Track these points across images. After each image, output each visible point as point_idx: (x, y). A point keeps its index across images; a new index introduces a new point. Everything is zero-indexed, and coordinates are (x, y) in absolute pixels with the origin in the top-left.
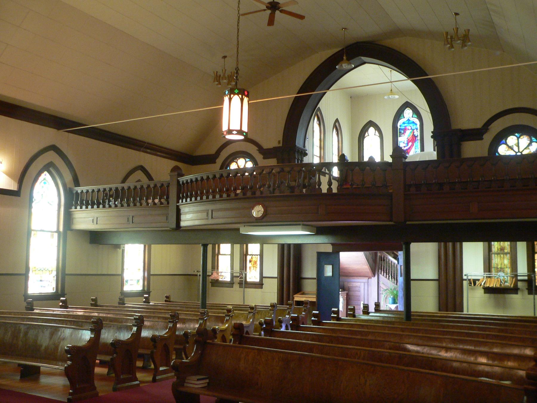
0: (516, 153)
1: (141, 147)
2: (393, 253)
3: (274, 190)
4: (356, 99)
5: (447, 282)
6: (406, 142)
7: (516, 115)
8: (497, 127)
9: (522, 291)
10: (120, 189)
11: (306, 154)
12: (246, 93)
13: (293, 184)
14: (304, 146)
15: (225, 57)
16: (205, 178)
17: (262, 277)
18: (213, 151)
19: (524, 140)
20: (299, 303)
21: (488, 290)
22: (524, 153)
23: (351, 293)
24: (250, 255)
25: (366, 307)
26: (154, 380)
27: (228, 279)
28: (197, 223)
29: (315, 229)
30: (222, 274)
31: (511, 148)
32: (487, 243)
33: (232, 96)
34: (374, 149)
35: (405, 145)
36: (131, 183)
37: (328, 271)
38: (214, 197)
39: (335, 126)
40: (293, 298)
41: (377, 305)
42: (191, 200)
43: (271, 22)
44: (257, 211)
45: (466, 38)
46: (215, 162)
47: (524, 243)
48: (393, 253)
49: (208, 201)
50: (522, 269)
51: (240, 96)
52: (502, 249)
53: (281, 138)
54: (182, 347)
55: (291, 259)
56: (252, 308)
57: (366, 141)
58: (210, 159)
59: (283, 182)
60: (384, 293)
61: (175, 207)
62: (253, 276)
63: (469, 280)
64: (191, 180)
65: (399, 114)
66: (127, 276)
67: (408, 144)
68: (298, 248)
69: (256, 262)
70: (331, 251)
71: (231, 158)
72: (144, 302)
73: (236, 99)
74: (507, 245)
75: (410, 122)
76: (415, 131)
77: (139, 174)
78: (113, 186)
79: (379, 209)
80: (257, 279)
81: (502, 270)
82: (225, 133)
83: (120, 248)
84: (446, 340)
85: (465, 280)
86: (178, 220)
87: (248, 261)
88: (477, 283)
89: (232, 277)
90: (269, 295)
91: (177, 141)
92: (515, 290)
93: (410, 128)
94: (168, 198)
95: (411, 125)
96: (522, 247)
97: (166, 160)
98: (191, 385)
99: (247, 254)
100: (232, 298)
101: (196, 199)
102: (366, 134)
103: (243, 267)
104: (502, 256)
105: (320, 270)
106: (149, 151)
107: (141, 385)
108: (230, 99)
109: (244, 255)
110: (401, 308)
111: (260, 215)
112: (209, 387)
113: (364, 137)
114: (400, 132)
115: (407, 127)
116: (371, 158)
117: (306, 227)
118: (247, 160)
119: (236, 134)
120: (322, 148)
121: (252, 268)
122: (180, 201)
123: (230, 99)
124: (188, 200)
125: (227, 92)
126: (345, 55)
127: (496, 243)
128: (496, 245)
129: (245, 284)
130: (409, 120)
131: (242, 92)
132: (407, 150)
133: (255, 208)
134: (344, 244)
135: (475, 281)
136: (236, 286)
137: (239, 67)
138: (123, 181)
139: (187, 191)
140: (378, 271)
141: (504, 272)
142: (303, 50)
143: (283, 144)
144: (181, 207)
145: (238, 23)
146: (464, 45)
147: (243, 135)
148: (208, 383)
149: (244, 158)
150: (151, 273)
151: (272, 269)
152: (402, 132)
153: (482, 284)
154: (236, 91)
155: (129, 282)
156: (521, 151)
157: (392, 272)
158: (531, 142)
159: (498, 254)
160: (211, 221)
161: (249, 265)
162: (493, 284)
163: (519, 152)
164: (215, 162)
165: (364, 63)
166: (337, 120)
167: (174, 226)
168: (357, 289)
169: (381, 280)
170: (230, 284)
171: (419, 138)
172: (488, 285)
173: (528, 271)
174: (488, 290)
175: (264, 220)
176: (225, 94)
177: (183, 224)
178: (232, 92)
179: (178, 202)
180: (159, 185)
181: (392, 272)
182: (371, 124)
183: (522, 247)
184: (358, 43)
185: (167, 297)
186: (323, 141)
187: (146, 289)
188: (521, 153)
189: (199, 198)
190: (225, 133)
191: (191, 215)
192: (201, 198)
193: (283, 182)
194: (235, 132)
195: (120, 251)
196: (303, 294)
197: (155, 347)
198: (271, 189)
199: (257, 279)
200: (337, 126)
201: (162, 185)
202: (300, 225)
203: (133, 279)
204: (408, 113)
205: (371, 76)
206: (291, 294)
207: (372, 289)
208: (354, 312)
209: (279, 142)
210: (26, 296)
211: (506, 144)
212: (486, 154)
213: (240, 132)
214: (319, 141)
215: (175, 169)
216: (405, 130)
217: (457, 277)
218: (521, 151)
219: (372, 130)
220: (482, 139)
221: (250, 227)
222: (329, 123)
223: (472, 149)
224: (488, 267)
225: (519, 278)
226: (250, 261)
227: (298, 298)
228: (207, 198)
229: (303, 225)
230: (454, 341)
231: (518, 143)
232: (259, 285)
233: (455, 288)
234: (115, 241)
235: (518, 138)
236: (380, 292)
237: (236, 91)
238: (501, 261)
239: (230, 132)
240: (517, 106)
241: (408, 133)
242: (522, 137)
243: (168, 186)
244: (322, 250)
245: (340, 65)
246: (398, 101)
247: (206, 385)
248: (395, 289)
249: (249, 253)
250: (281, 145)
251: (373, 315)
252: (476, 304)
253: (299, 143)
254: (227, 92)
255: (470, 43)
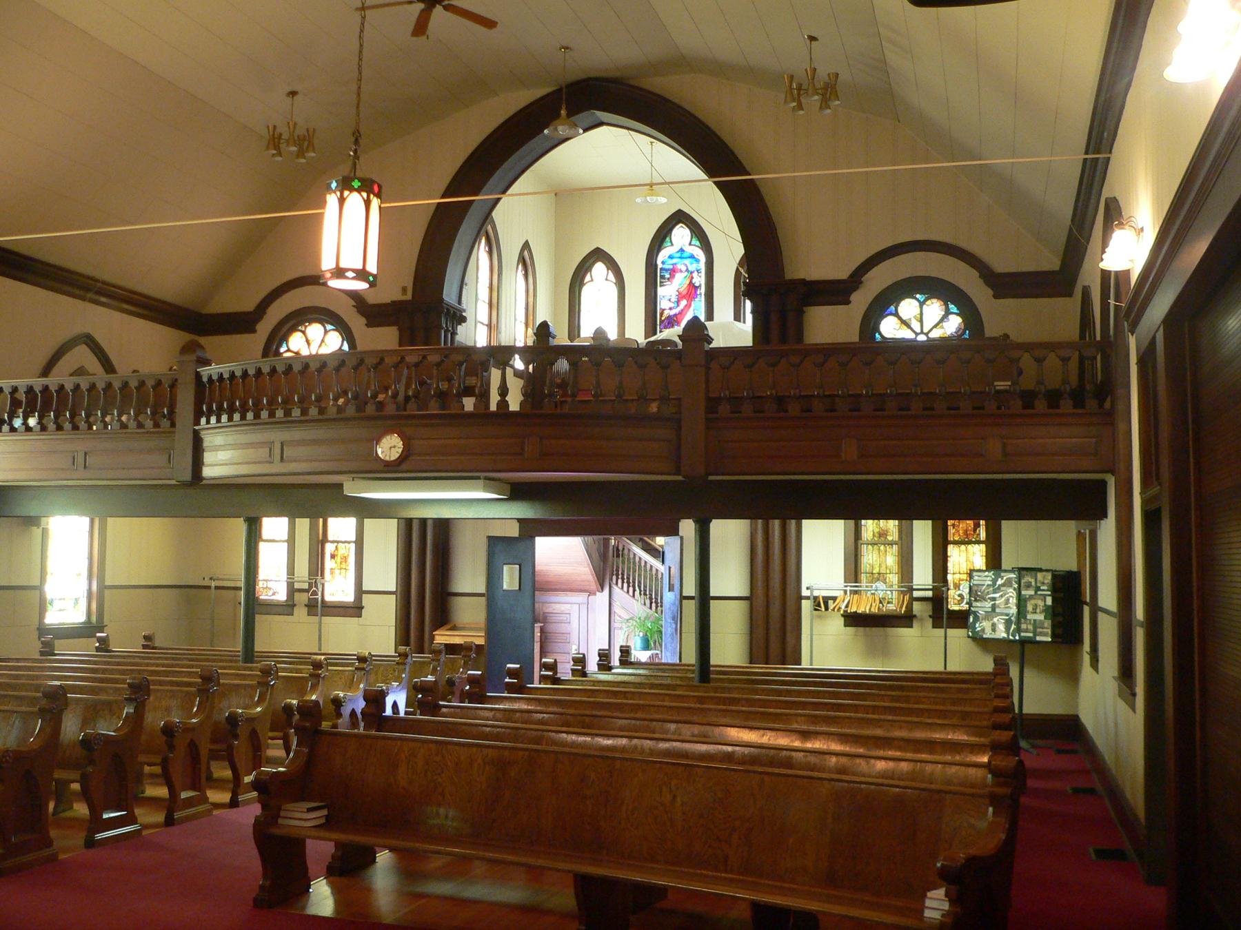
0: (917, 334)
1: (88, 290)
2: (641, 540)
3: (407, 399)
4: (568, 199)
5: (768, 601)
6: (674, 299)
7: (962, 265)
8: (878, 279)
9: (922, 620)
10: (37, 389)
11: (463, 319)
12: (376, 188)
13: (444, 386)
14: (460, 302)
15: (293, 94)
16: (251, 372)
17: (360, 591)
18: (249, 305)
19: (934, 309)
20: (451, 649)
21: (854, 620)
22: (932, 335)
23: (551, 628)
24: (333, 542)
25: (581, 661)
26: (169, 822)
27: (282, 596)
28: (244, 470)
29: (508, 487)
30: (270, 584)
31: (905, 323)
32: (851, 523)
33: (346, 193)
34: (604, 313)
35: (672, 305)
36: (60, 377)
37: (509, 578)
38: (288, 413)
39: (522, 260)
40: (432, 638)
41: (625, 651)
42: (219, 421)
43: (420, 28)
44: (390, 447)
45: (829, 91)
46: (254, 331)
47: (928, 524)
48: (641, 540)
49: (273, 423)
50: (923, 576)
51: (365, 195)
52: (883, 534)
53: (409, 282)
54: (224, 746)
55: (428, 552)
56: (362, 659)
57: (587, 293)
58: (243, 323)
59: (416, 382)
60: (624, 626)
61: (191, 436)
62: (338, 588)
63: (816, 598)
64: (221, 376)
65: (662, 236)
66: (50, 590)
67: (678, 303)
68: (444, 527)
69: (345, 559)
70: (517, 535)
71: (291, 323)
72: (98, 649)
73: (355, 200)
74: (892, 525)
75: (685, 255)
76: (695, 275)
77: (81, 356)
78: (22, 383)
79: (616, 441)
80: (349, 597)
81: (881, 577)
82: (328, 275)
83: (38, 525)
84: (799, 719)
85: (808, 598)
86: (198, 463)
87: (327, 556)
88: (831, 604)
89: (292, 591)
90: (377, 633)
91: (169, 279)
92: (906, 619)
93: (684, 268)
94: (172, 412)
95: (687, 261)
96: (922, 531)
97: (141, 322)
98: (292, 823)
99: (325, 540)
100: (284, 638)
101: (243, 417)
102: (588, 278)
103: (317, 568)
104: (882, 548)
105: (493, 577)
106: (103, 299)
107: (145, 833)
108: (342, 201)
109: (318, 543)
110: (691, 657)
111: (394, 455)
112: (329, 824)
113: (582, 284)
114: (662, 277)
115: (679, 266)
116: (600, 334)
117: (491, 483)
118: (329, 327)
119: (353, 278)
120: (494, 305)
121: (337, 572)
122: (203, 420)
123: (342, 201)
124: (213, 420)
125: (334, 185)
126: (564, 107)
127: (870, 522)
128: (870, 527)
129: (319, 608)
130: (682, 250)
131: (369, 187)
132: (675, 315)
133: (384, 440)
134: (559, 521)
135: (826, 600)
136: (301, 612)
137: (362, 132)
138: (46, 372)
139: (218, 399)
140: (611, 579)
141: (884, 581)
142: (469, 86)
143: (413, 296)
144: (203, 434)
145: (362, 31)
146: (825, 104)
147: (367, 281)
148: (327, 816)
149: (322, 322)
150: (107, 583)
151: (384, 572)
152: (667, 276)
153: (843, 607)
154: (356, 184)
155: (55, 603)
156: (925, 330)
157: (639, 582)
158: (948, 313)
159: (873, 544)
160: (277, 467)
161: (329, 564)
162: (864, 606)
163: (922, 332)
164: (254, 331)
165: (601, 124)
166: (526, 245)
167: (187, 476)
168: (563, 617)
169: (615, 597)
170: (287, 608)
171: (703, 290)
172: (854, 610)
173: (934, 581)
174: (854, 620)
175: (404, 466)
176: (328, 189)
177: (207, 472)
178: (346, 185)
179: (197, 423)
180: (150, 383)
181: (639, 582)
182: (598, 255)
183: (922, 531)
184: (589, 79)
185: (146, 638)
186: (495, 290)
187: (94, 619)
188: (927, 334)
189: (250, 415)
190: (328, 275)
191: (225, 453)
192: (257, 416)
193: (416, 382)
194: (350, 274)
195: (37, 532)
196: (454, 628)
197: (171, 747)
198: (401, 397)
199: (349, 597)
200: (525, 261)
201: (142, 384)
202: (478, 478)
203: (66, 599)
204: (681, 234)
205: (611, 155)
206: (427, 629)
207: (601, 614)
208: (584, 667)
209: (404, 290)
210: (42, 630)
211: (896, 315)
212: (855, 338)
213: (362, 274)
214: (487, 291)
215: (187, 349)
216: (673, 272)
217: (788, 592)
218: (925, 330)
219: (599, 269)
220: (848, 302)
221: (365, 482)
222: (510, 251)
223: (827, 325)
224: (853, 570)
225: (916, 594)
226: (333, 556)
227: (442, 637)
228: (272, 415)
229: (486, 478)
230: (815, 720)
231: (921, 314)
232: (355, 609)
233: (784, 616)
234: (32, 509)
235: (922, 304)
236: (615, 625)
237: (356, 184)
238: (880, 559)
239: (339, 273)
240: (920, 236)
241: (680, 281)
242: (929, 302)
243: (173, 386)
244: (497, 532)
245: (551, 128)
246: (664, 206)
247: (323, 821)
248: (647, 618)
249: (330, 538)
250: (409, 296)
251: (619, 672)
252: (826, 647)
253: (449, 295)
254: (334, 185)
255: (837, 103)
